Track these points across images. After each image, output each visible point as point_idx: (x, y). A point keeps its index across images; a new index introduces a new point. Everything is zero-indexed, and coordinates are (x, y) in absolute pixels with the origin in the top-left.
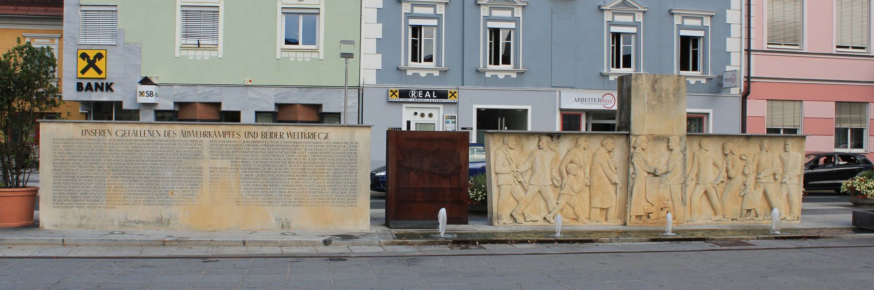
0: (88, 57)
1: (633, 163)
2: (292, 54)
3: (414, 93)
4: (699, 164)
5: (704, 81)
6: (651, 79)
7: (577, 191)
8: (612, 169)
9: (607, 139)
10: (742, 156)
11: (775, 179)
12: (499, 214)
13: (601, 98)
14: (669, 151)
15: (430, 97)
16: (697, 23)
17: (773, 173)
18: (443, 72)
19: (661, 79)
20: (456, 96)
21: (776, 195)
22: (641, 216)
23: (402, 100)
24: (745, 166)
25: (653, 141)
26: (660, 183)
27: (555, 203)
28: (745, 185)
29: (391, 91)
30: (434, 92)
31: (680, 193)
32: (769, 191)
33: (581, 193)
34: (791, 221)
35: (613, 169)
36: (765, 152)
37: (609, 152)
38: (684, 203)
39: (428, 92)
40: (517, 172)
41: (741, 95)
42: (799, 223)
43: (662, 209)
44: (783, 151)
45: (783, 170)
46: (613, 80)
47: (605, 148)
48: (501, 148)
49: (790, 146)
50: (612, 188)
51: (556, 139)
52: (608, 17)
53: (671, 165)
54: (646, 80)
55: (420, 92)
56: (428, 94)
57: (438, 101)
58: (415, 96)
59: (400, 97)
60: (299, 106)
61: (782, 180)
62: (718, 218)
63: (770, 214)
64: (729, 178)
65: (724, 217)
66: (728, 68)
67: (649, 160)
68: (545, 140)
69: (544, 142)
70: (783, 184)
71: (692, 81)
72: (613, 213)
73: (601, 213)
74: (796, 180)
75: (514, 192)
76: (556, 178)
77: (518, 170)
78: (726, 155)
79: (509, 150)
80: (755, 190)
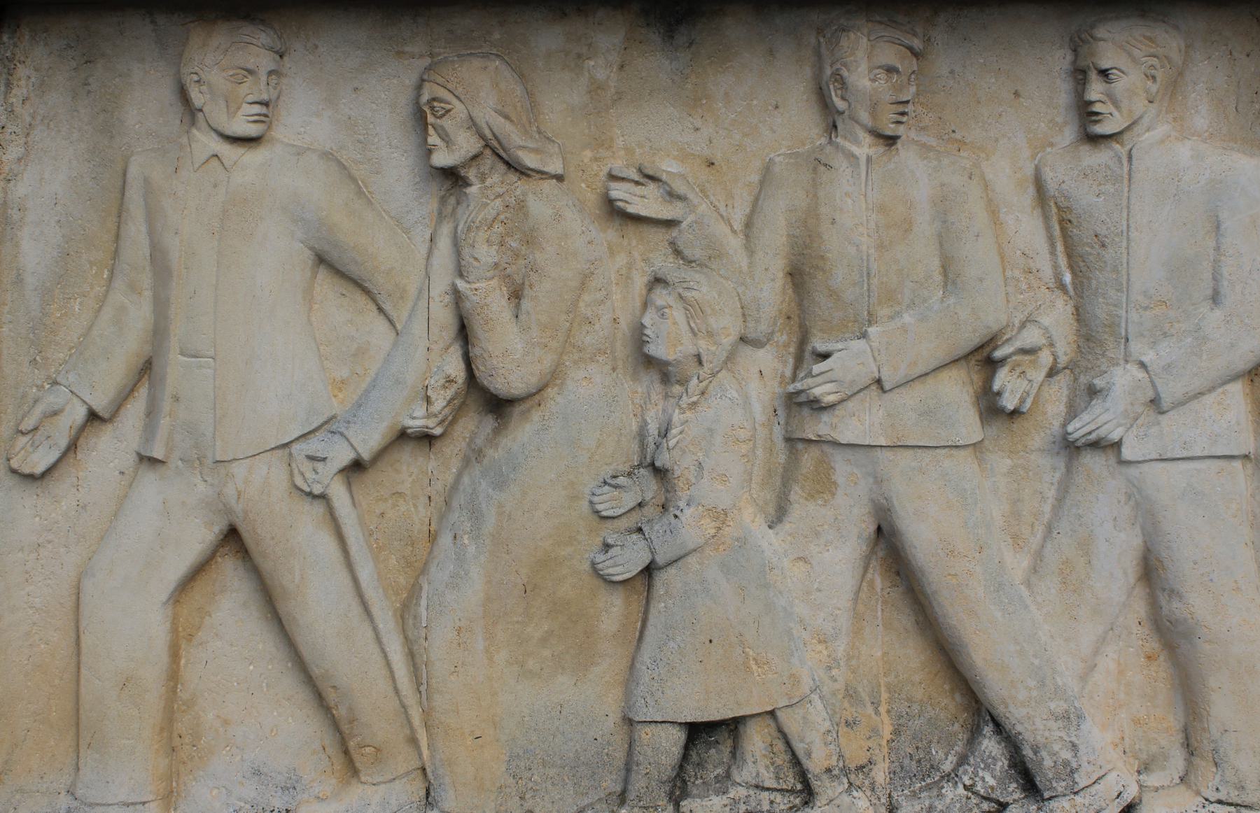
10: (619, 191)
17: (969, 338)
21: (1017, 564)
24: (658, 281)
36: (864, 147)
44: (1069, 134)
49: (1129, 81)
63: (963, 760)
68: (77, 591)
70: (1093, 462)
80: (779, 515)
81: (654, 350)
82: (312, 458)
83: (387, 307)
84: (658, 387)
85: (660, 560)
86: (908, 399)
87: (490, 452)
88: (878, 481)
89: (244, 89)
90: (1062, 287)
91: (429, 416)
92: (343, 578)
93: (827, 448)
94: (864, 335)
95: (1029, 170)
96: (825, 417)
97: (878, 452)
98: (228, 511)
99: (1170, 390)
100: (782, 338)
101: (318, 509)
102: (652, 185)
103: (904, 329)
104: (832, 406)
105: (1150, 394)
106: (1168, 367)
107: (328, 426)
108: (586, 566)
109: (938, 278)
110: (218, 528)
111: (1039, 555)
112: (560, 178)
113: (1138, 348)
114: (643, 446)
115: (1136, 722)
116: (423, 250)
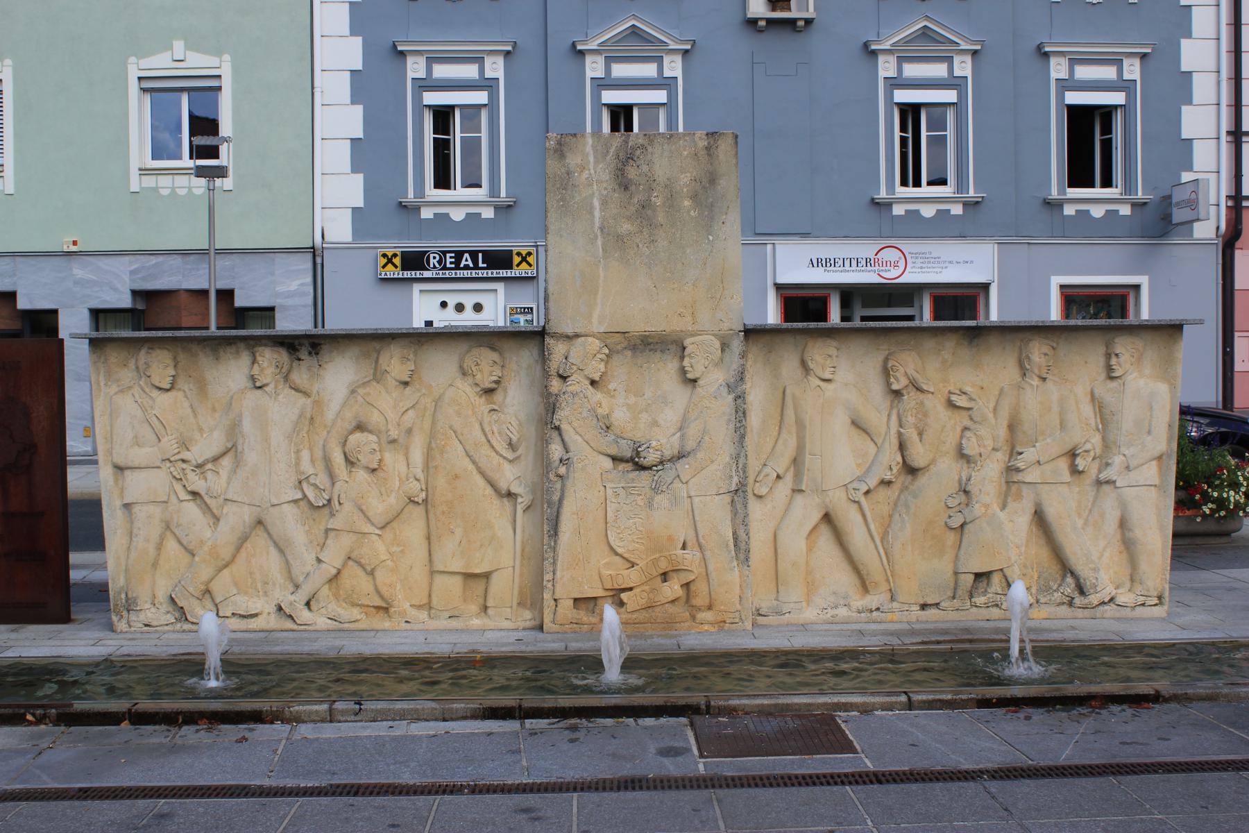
0: (522, 255)
1: (558, 428)
2: (165, 181)
3: (434, 258)
4: (800, 425)
5: (1125, 210)
6: (612, 150)
7: (380, 521)
8: (498, 447)
9: (475, 352)
10: (954, 398)
11: (1075, 471)
12: (130, 596)
13: (872, 256)
14: (690, 386)
15: (471, 265)
16: (1109, 73)
17: (1068, 447)
18: (504, 209)
19: (650, 149)
20: (531, 262)
21: (1080, 522)
22: (595, 598)
23: (407, 274)
24: (966, 429)
25: (629, 353)
26: (656, 490)
27: (310, 558)
28: (966, 492)
29: (384, 255)
30: (480, 255)
31: (729, 522)
32: (1052, 512)
33: (394, 524)
34: (1133, 608)
35: (501, 446)
37: (489, 392)
38: (742, 556)
39: (466, 255)
40: (183, 461)
41: (1221, 239)
42: (1164, 615)
43: (665, 576)
44: (1103, 376)
45: (1104, 439)
46: (903, 213)
47: (470, 380)
48: (130, 388)
50: (497, 513)
51: (310, 353)
52: (886, 68)
53: (693, 430)
54: (595, 151)
55: (448, 255)
56: (467, 260)
57: (490, 275)
58: (437, 265)
59: (404, 269)
60: (184, 296)
61: (1100, 471)
62: (872, 600)
63: (1060, 585)
64: (911, 470)
65: (892, 599)
66: (1186, 177)
67: (620, 417)
69: (265, 365)
70: (1106, 488)
71: (1097, 212)
72: (505, 586)
73: (465, 588)
74: (1150, 473)
75: (178, 525)
76: (312, 480)
77: (186, 455)
78: (897, 394)
79: (155, 393)
80: (1003, 507)
81: (965, 452)
82: (854, 489)
83: (875, 439)
84: (965, 466)
85: (968, 521)
86: (1047, 468)
87: (911, 487)
88: (1037, 495)
89: (828, 362)
90: (1098, 430)
91: (892, 475)
92: (865, 529)
93: (1021, 484)
94: (1034, 446)
95: (1089, 390)
96: (1020, 474)
97: (1037, 485)
98: (827, 507)
99: (1133, 463)
100: (1005, 448)
101: (856, 506)
102: (964, 396)
103: (1048, 444)
104: (1023, 470)
105: (1126, 465)
106: (1132, 456)
107: (860, 479)
108: (943, 523)
109: (1059, 427)
110: (822, 513)
111: (1087, 520)
112: (933, 393)
113: (1123, 450)
114: (960, 484)
115: (1115, 573)
116: (886, 419)
